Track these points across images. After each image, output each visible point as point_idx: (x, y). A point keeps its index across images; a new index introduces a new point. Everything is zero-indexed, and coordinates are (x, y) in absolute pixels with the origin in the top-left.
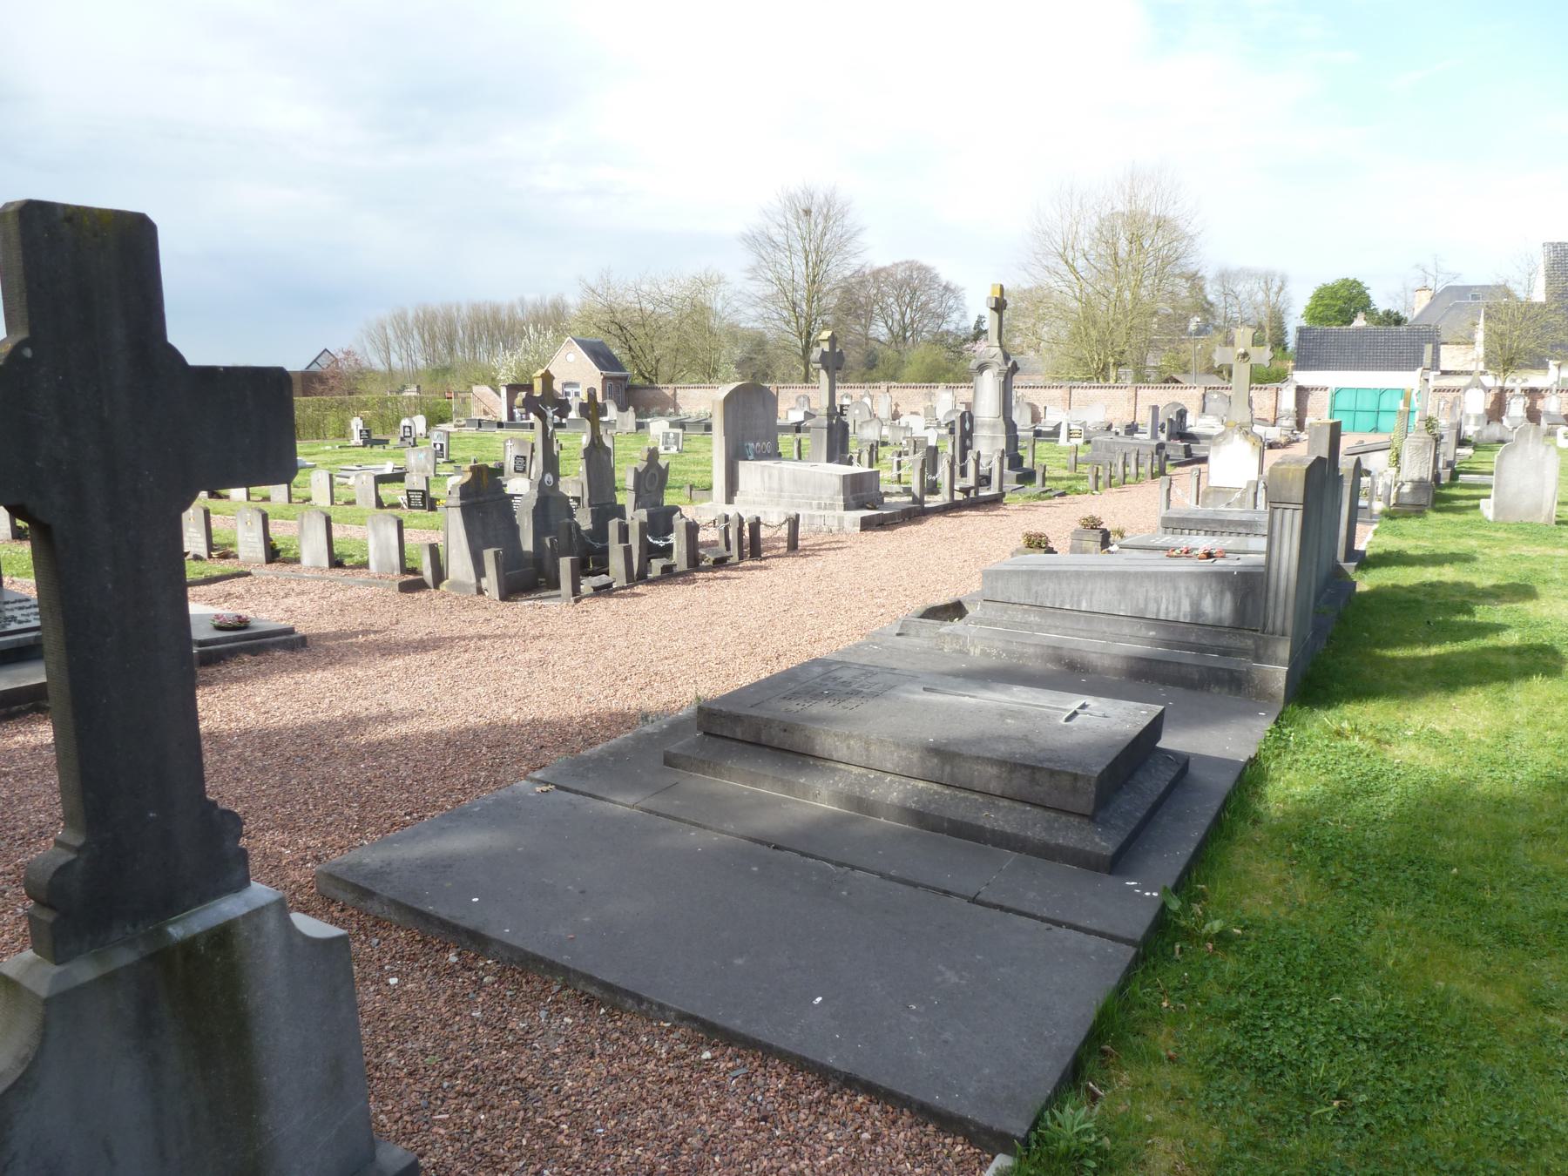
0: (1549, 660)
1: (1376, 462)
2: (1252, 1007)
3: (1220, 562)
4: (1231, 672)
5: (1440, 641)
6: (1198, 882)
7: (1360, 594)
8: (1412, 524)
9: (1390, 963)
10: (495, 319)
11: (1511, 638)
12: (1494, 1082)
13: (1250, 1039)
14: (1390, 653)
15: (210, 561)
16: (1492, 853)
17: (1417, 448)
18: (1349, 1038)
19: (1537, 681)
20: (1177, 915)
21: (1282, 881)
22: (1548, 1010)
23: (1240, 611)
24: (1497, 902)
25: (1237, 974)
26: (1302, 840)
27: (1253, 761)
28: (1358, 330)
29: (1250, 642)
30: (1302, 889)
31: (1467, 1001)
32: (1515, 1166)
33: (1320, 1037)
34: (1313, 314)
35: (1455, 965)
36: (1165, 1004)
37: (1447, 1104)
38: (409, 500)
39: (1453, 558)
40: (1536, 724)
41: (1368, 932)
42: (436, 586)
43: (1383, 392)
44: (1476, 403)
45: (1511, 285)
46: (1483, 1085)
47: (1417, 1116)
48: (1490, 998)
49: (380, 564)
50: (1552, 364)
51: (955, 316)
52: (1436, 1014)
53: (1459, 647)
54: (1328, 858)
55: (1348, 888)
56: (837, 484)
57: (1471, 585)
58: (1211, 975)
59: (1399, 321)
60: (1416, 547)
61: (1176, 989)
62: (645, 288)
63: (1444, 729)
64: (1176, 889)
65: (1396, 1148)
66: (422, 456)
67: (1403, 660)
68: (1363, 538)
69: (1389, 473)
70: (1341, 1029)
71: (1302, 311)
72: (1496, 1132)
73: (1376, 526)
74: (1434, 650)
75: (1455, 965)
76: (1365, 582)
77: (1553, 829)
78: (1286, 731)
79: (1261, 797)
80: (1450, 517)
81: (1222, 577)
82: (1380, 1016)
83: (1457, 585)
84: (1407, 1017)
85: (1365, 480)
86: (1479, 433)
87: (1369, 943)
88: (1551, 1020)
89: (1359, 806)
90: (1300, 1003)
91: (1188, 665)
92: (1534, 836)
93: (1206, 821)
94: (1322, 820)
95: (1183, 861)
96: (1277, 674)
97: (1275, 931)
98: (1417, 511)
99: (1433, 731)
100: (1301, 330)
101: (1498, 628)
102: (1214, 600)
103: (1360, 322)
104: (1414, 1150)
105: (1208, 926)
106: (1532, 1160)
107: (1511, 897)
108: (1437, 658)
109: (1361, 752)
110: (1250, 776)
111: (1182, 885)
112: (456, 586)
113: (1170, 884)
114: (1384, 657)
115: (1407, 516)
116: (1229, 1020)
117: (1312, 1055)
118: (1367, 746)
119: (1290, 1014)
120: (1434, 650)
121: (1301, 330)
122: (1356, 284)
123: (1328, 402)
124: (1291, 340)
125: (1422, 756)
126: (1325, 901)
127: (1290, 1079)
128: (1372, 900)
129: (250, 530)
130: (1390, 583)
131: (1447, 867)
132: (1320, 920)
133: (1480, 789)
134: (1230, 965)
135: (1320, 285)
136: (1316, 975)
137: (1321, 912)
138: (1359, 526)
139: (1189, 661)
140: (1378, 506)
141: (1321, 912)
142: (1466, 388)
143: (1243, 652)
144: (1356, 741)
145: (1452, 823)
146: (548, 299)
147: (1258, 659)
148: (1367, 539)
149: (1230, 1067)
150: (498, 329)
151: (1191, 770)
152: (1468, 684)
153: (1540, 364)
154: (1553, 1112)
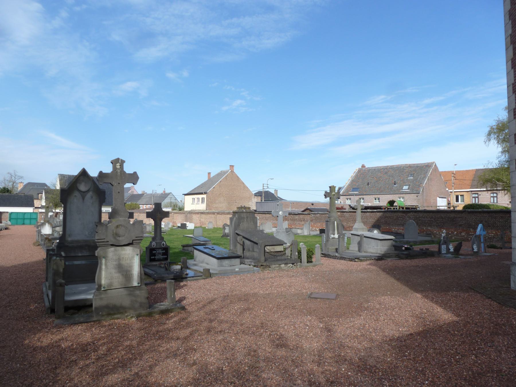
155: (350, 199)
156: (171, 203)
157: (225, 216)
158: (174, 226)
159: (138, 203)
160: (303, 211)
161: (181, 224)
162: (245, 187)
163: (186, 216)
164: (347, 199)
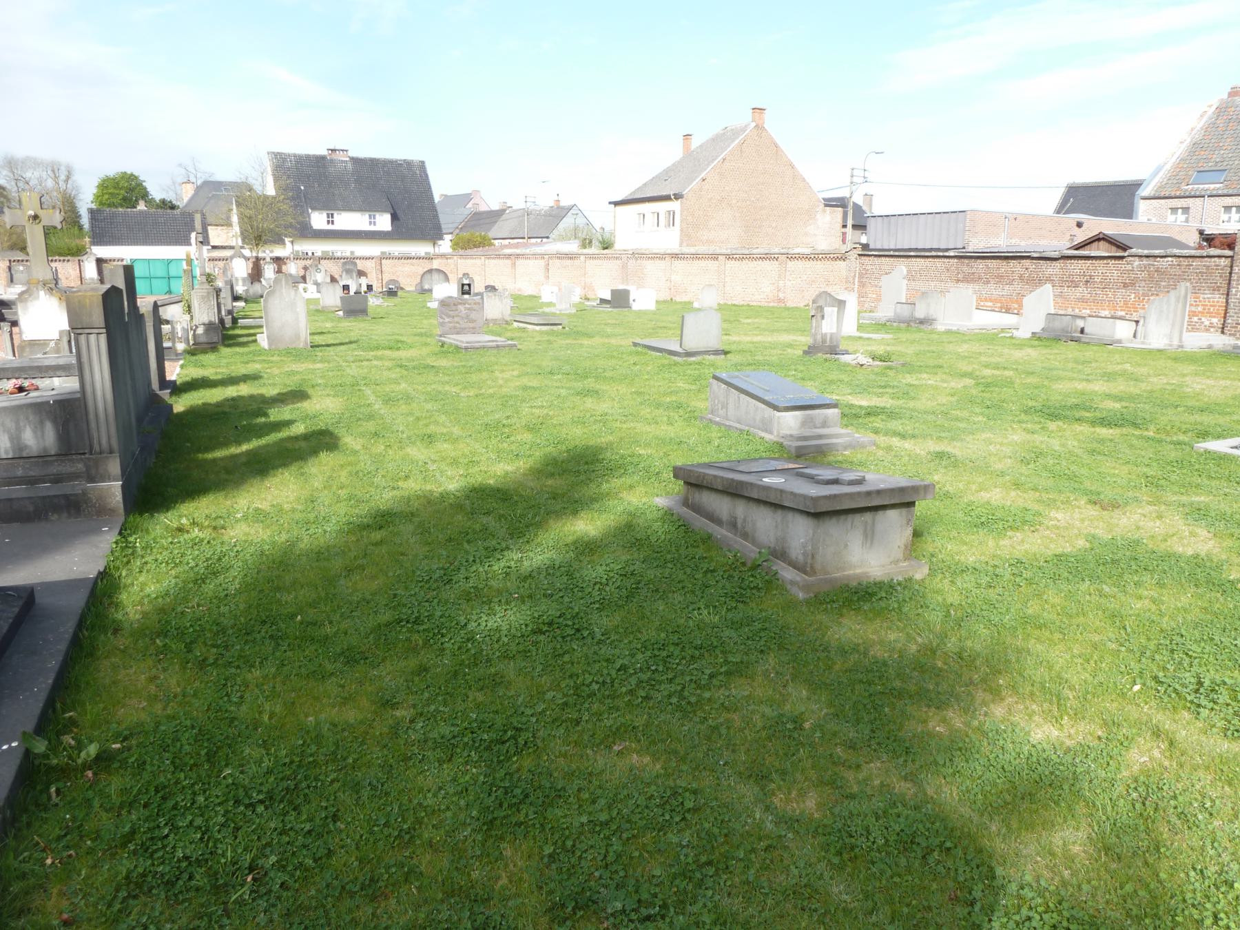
0: (327, 439)
1: (172, 312)
2: (146, 820)
3: (33, 394)
4: (66, 497)
5: (248, 440)
6: (64, 712)
7: (179, 415)
8: (210, 358)
9: (266, 718)
11: (299, 429)
12: (374, 788)
13: (152, 856)
14: (210, 456)
16: (323, 594)
17: (203, 297)
18: (247, 807)
19: (324, 456)
20: (46, 756)
21: (153, 679)
22: (394, 706)
23: (64, 437)
24: (336, 633)
25: (124, 791)
26: (164, 633)
27: (103, 575)
28: (141, 212)
29: (80, 466)
30: (173, 680)
31: (335, 726)
32: (407, 854)
33: (220, 819)
34: (98, 198)
35: (316, 699)
36: (49, 861)
37: (342, 826)
39: (245, 378)
40: (331, 486)
41: (242, 697)
43: (169, 262)
44: (241, 269)
45: (251, 181)
46: (365, 793)
47: (322, 852)
48: (351, 715)
50: (287, 240)
52: (314, 748)
53: (263, 441)
54: (192, 642)
55: (215, 664)
57: (262, 396)
58: (96, 803)
59: (173, 207)
60: (216, 373)
61: (59, 838)
63: (264, 506)
64: (40, 730)
65: (313, 892)
67: (222, 459)
68: (172, 373)
69: (183, 321)
70: (237, 802)
71: (91, 198)
72: (386, 831)
73: (181, 362)
74: (245, 447)
75: (316, 699)
76: (180, 405)
77: (360, 562)
78: (131, 539)
79: (117, 605)
80: (238, 349)
81: (40, 408)
82: (269, 772)
83: (252, 397)
84: (292, 762)
85: (166, 328)
86: (247, 291)
87: (244, 708)
88: (398, 713)
89: (209, 588)
90: (194, 794)
91: (18, 499)
92: (349, 571)
93: (63, 647)
94: (179, 609)
95: (43, 697)
96: (113, 490)
97: (155, 731)
98: (212, 347)
99: (257, 509)
100: (91, 211)
101: (288, 423)
102: (35, 432)
103: (142, 206)
104: (328, 886)
105: (83, 754)
106: (418, 842)
107: (344, 626)
108: (248, 452)
109: (202, 540)
110: (103, 589)
111: (49, 722)
113: (30, 726)
114: (206, 460)
115: (204, 352)
116: (124, 845)
117: (217, 840)
118: (205, 534)
119: (188, 809)
120: (245, 447)
121: (91, 211)
122: (132, 177)
124: (85, 221)
125: (253, 532)
126: (197, 684)
127: (200, 879)
128: (238, 667)
130: (200, 402)
131: (292, 616)
132: (196, 703)
133: (302, 546)
134: (115, 784)
135: (102, 176)
136: (203, 759)
137: (195, 695)
138: (167, 364)
139: (20, 495)
140: (180, 347)
141: (195, 695)
142: (232, 258)
143: (74, 476)
144: (196, 532)
145: (288, 579)
147: (92, 479)
148: (174, 372)
149: (135, 897)
151: (37, 600)
152: (275, 467)
153: (279, 241)
154: (421, 790)
155: (1186, 210)
156: (576, 229)
157: (752, 264)
158: (588, 299)
159: (491, 234)
160: (1078, 247)
161: (614, 292)
162: (797, 178)
163: (624, 267)
164: (1174, 210)
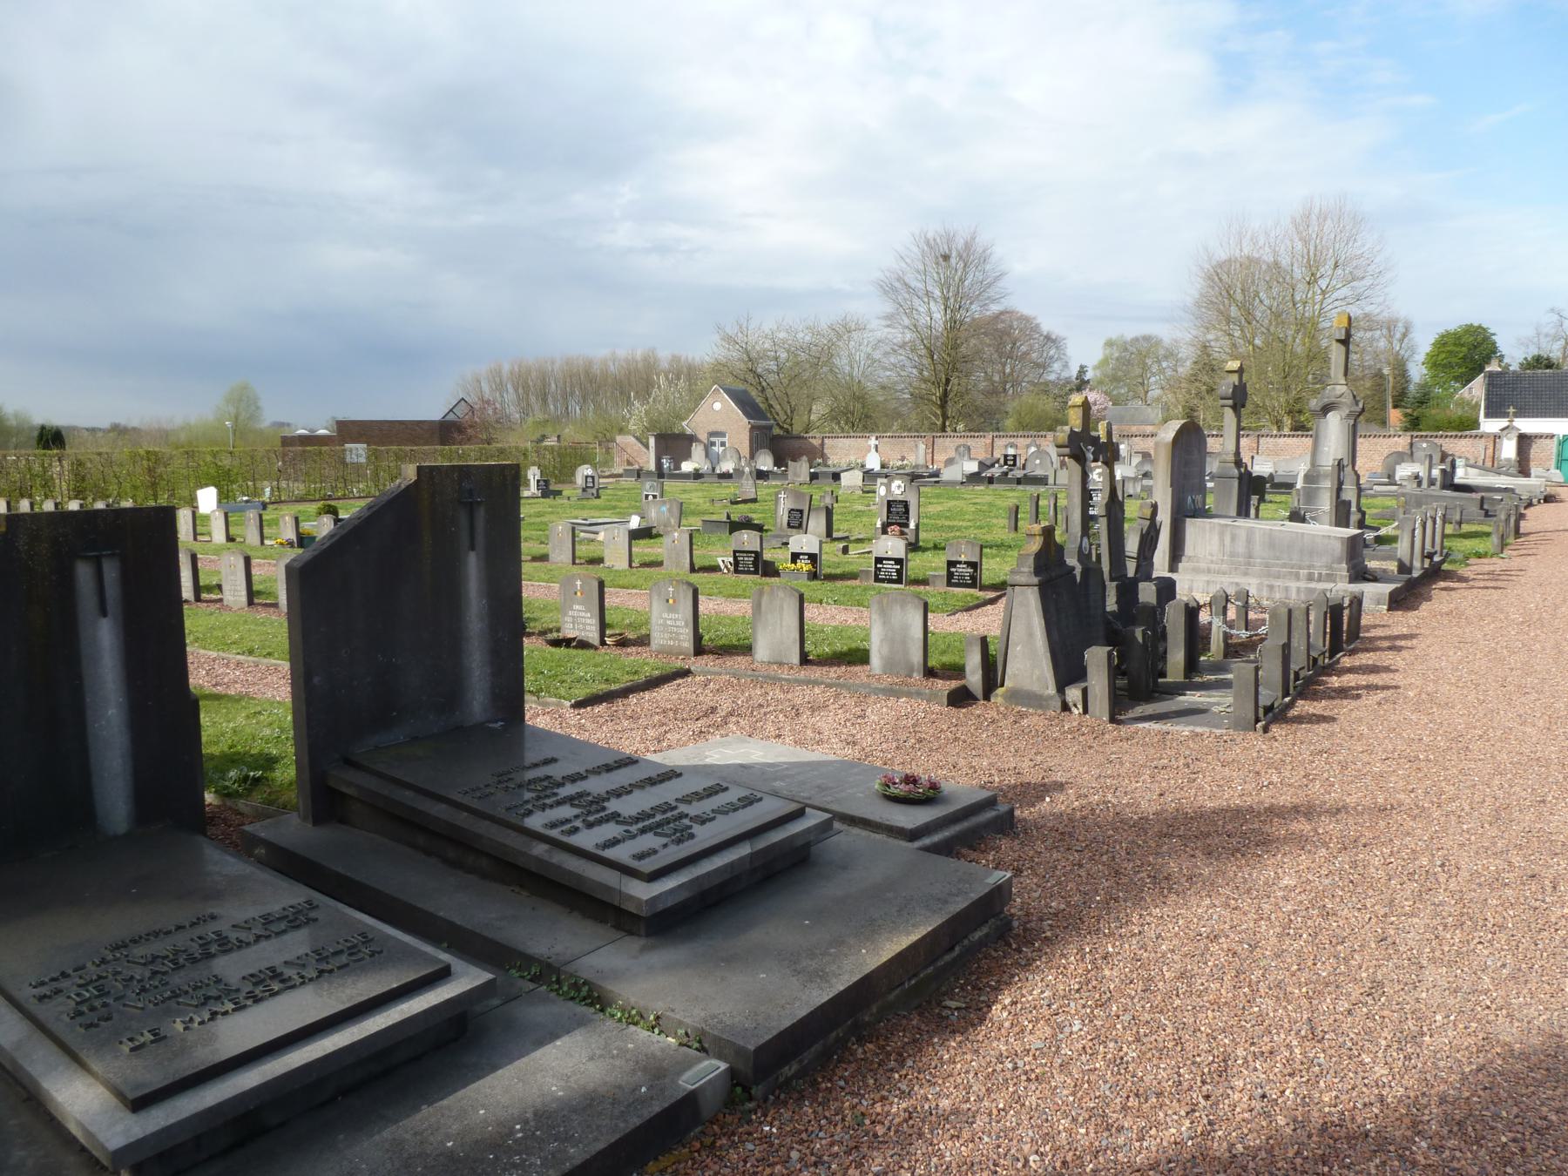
10: (587, 373)
15: (603, 650)
38: (736, 563)
42: (987, 697)
49: (889, 666)
51: (1056, 366)
56: (1338, 549)
62: (782, 335)
66: (664, 509)
112: (1020, 697)
123: (1555, 450)
129: (672, 609)
135: (1441, 330)
146: (639, 354)
150: (635, 381)
